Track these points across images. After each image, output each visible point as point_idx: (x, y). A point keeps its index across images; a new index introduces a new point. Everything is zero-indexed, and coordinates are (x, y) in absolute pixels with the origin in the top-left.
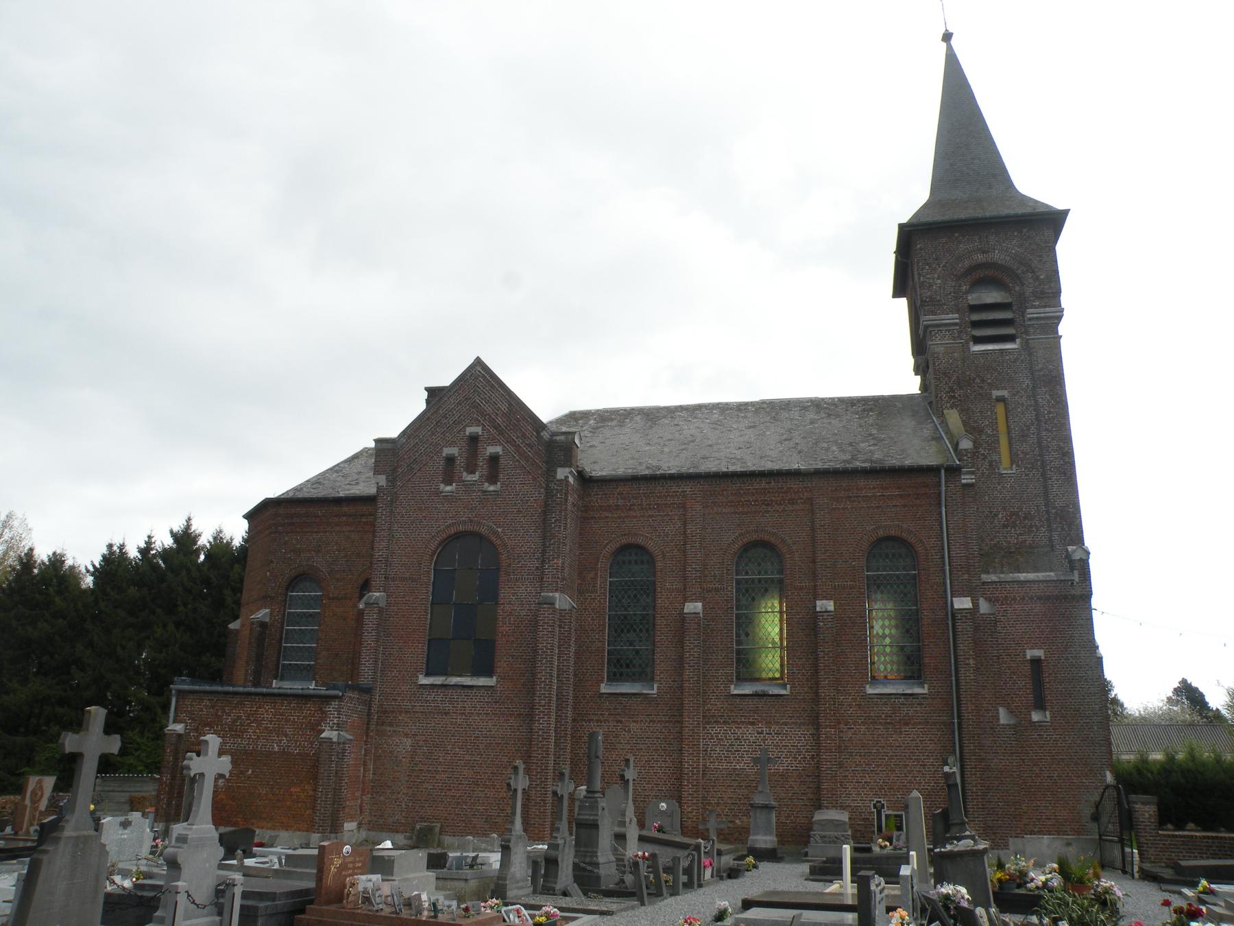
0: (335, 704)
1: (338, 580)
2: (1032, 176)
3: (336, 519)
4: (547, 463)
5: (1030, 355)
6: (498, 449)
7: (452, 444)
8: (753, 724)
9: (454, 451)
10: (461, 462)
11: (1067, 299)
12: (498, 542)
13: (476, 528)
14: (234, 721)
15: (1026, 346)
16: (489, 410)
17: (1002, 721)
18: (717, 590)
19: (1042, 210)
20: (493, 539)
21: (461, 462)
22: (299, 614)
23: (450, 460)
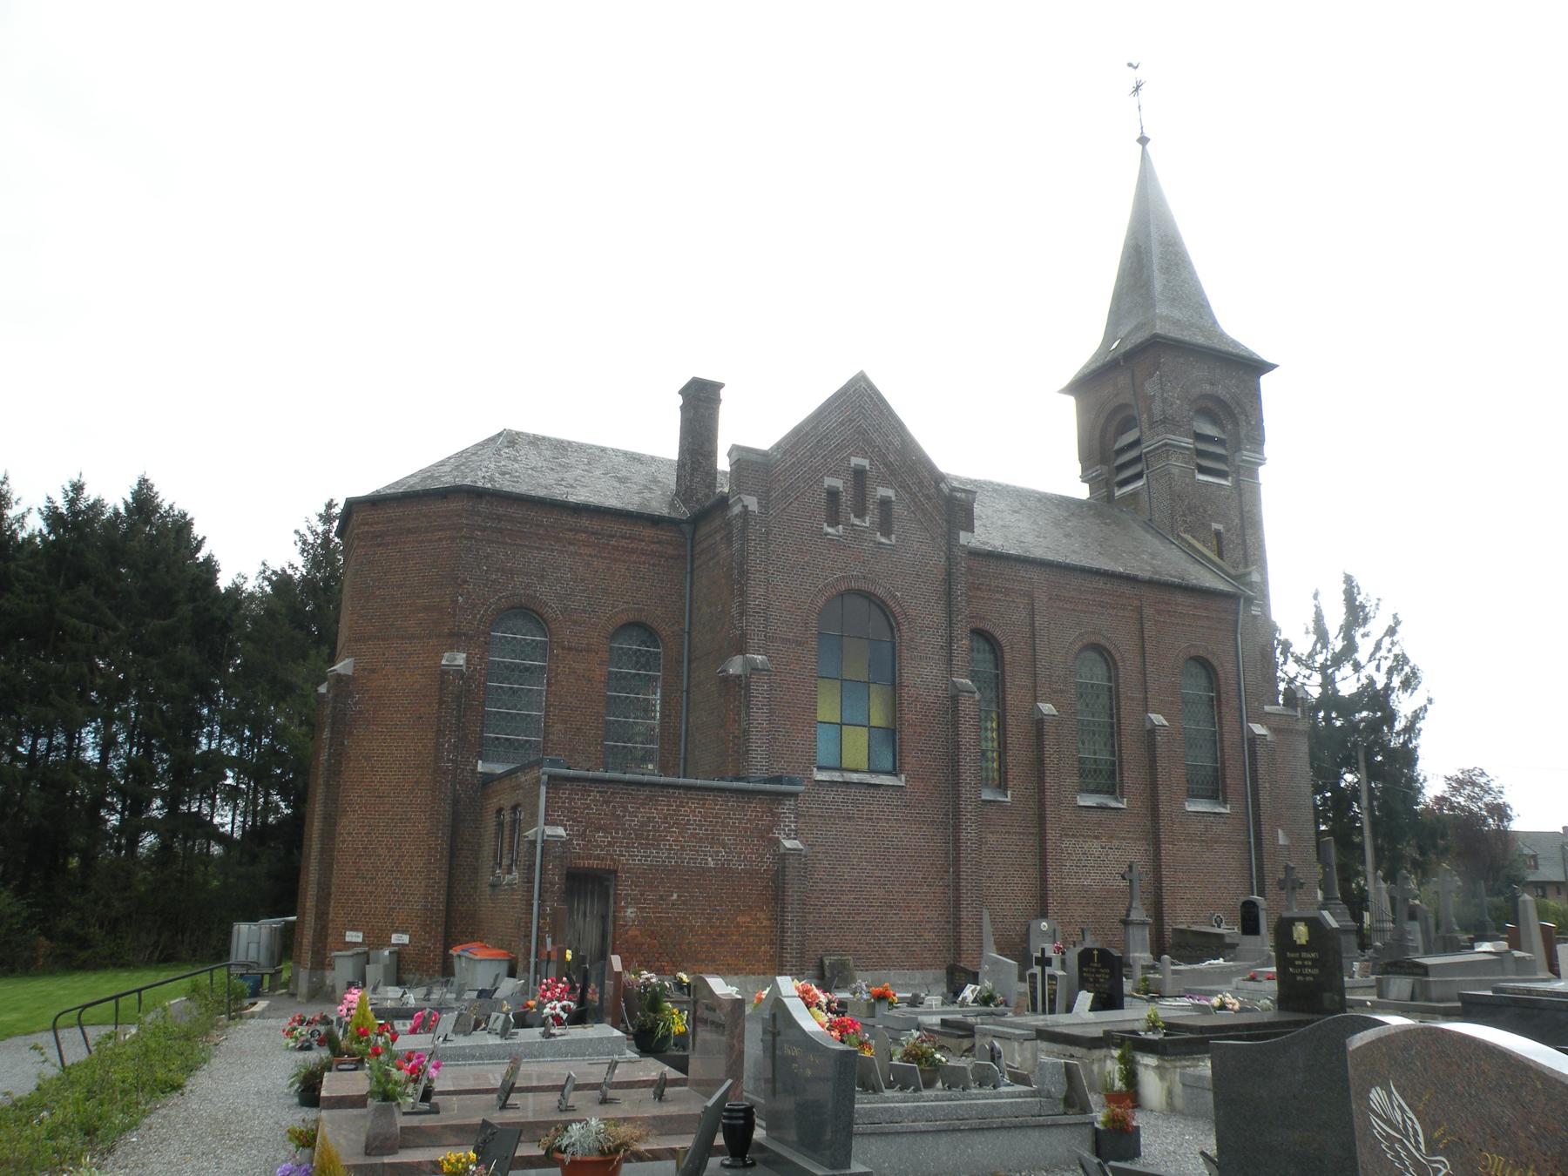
0: (790, 803)
1: (575, 623)
2: (1239, 320)
3: (570, 535)
4: (948, 522)
5: (1240, 495)
6: (890, 493)
7: (835, 474)
8: (1096, 837)
9: (838, 483)
10: (846, 499)
11: (1269, 448)
12: (897, 609)
13: (871, 588)
14: (643, 824)
15: (1237, 483)
16: (879, 441)
17: (1281, 842)
18: (1062, 691)
19: (1224, 347)
20: (891, 603)
21: (846, 499)
22: (507, 666)
23: (833, 494)
